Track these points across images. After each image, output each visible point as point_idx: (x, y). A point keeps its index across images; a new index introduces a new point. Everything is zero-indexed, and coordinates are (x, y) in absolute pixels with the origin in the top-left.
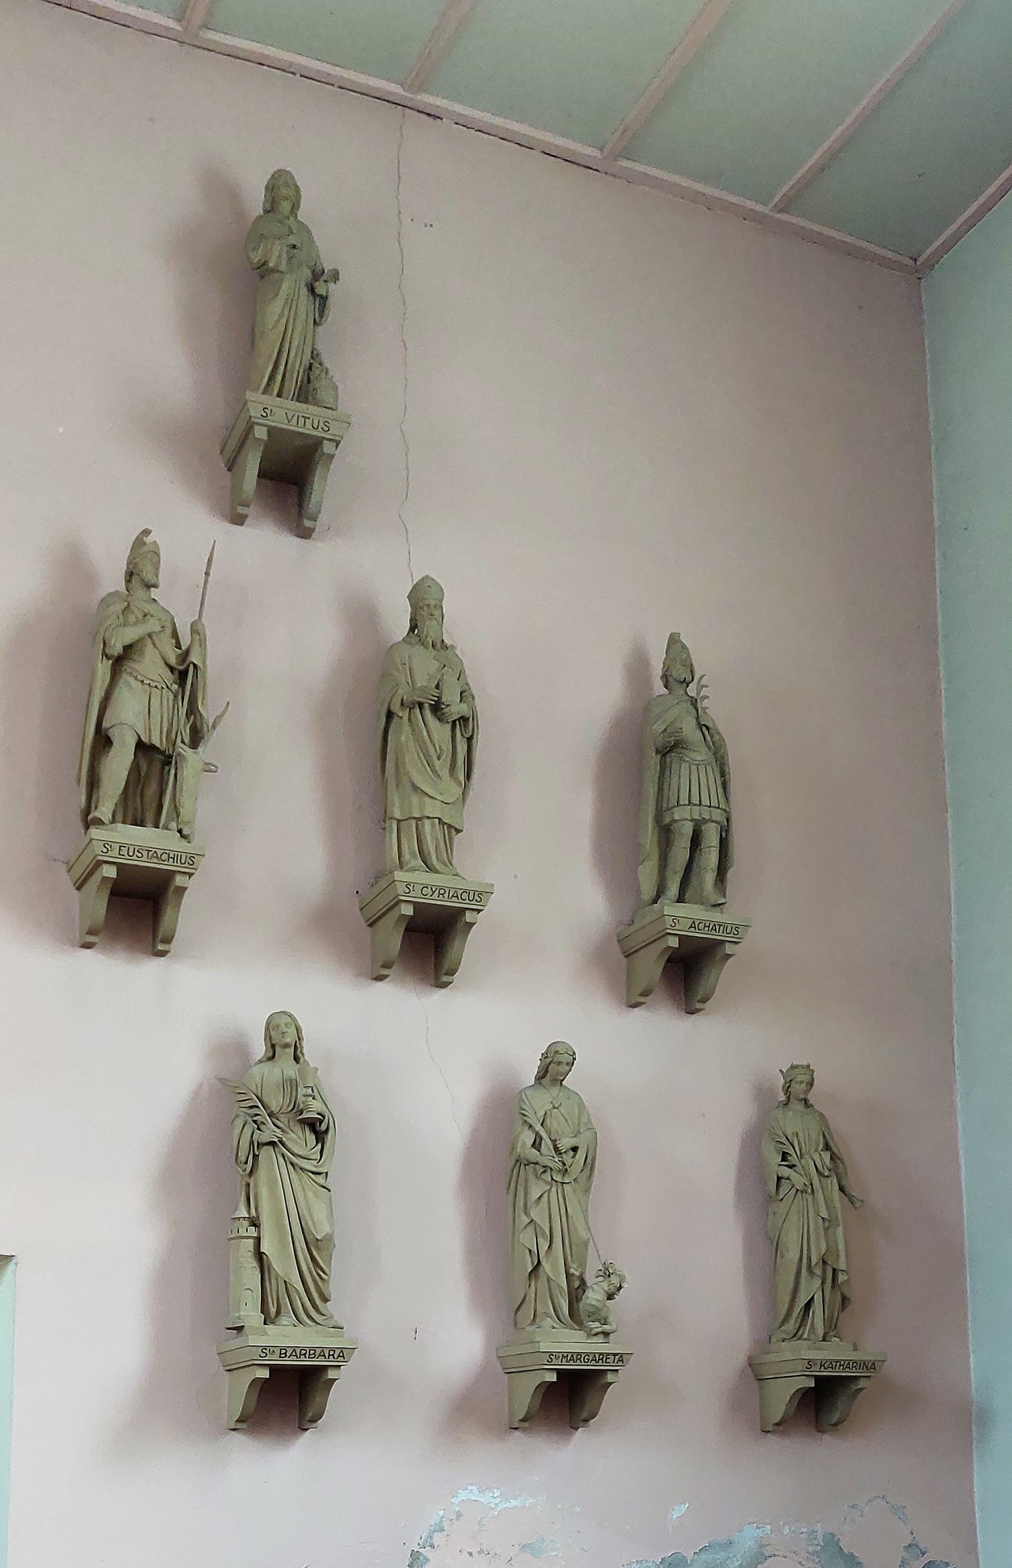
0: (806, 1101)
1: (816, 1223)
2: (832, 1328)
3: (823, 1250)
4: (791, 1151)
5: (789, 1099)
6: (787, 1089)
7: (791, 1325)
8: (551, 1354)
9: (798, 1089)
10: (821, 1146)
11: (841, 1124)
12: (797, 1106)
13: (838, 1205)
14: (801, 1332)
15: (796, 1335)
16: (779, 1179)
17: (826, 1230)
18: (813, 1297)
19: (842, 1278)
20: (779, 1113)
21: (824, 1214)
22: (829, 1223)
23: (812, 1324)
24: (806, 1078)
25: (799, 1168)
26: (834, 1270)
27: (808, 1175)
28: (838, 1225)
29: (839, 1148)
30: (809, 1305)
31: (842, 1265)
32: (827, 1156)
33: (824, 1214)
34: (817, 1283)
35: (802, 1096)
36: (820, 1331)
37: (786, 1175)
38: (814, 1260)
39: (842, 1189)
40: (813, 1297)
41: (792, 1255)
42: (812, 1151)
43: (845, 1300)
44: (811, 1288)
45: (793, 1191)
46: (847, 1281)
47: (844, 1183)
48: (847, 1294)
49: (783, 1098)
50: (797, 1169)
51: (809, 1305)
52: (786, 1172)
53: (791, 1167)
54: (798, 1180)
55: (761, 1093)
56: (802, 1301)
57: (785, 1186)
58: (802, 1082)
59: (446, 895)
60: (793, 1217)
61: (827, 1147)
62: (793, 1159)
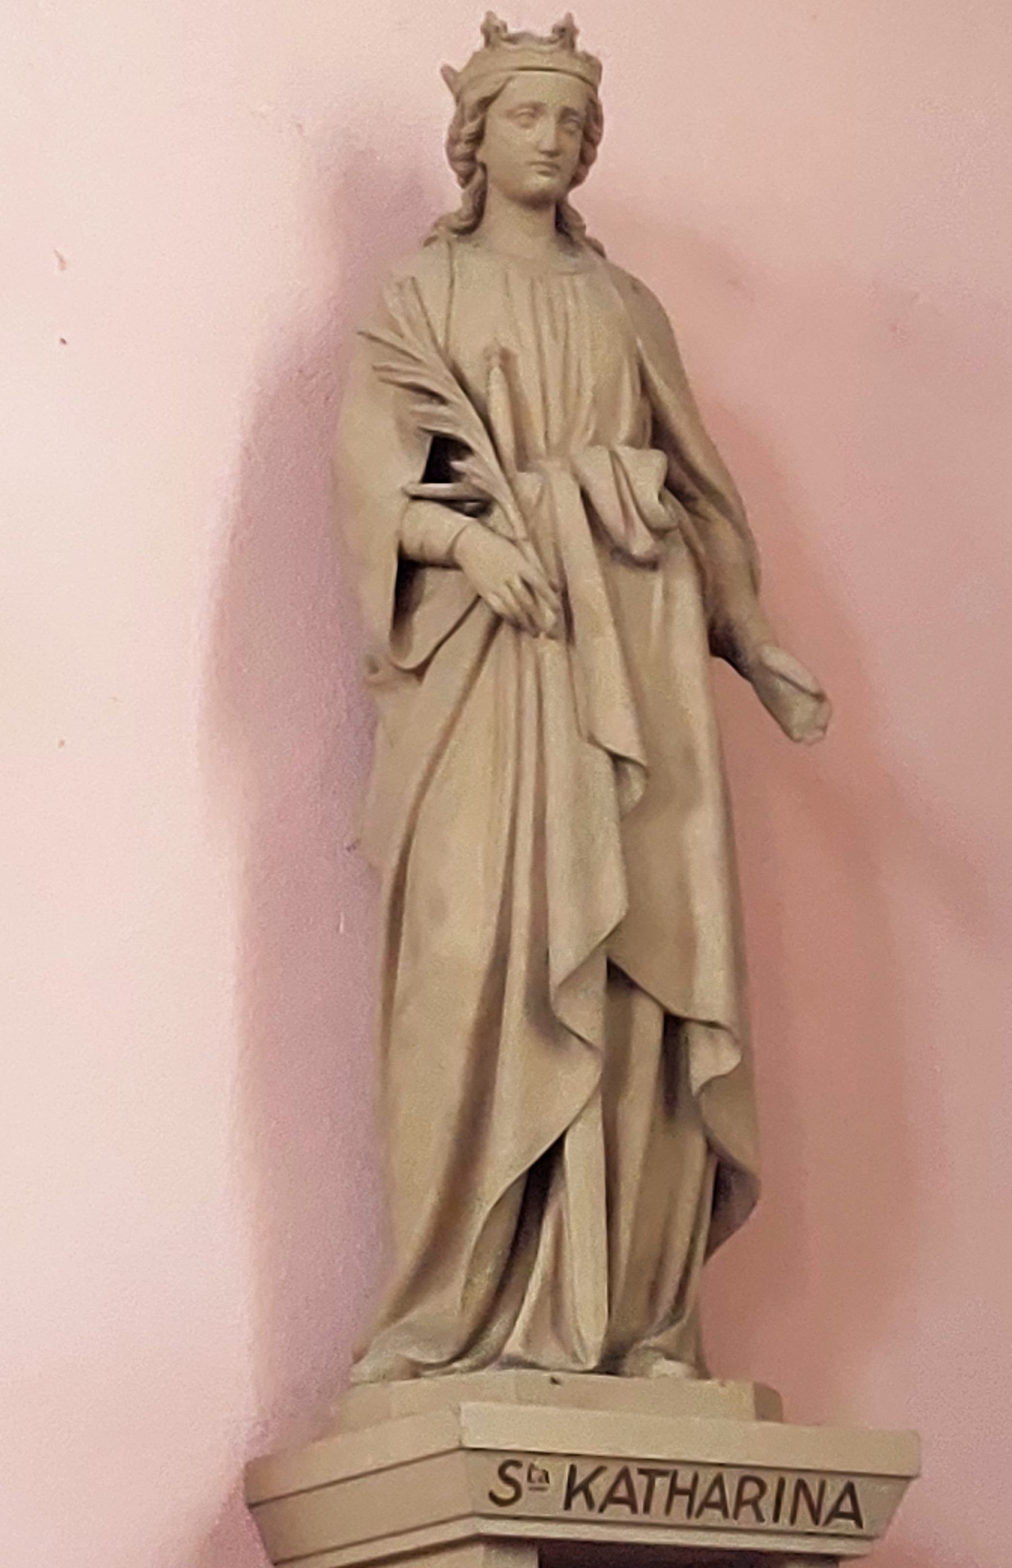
0: (564, 226)
1: (579, 776)
2: (655, 1317)
3: (612, 905)
4: (473, 436)
5: (479, 212)
6: (470, 151)
7: (451, 1303)
8: (507, 1464)
9: (521, 146)
10: (625, 425)
11: (741, 383)
12: (512, 230)
13: (697, 711)
14: (497, 1330)
15: (472, 1346)
16: (410, 569)
17: (630, 819)
18: (558, 1146)
19: (708, 1061)
20: (429, 268)
21: (622, 734)
22: (642, 784)
23: (555, 1284)
24: (553, 90)
25: (506, 511)
26: (674, 1026)
27: (535, 537)
28: (689, 803)
29: (716, 448)
30: (542, 1177)
31: (710, 994)
32: (648, 470)
33: (622, 734)
34: (583, 1075)
35: (539, 182)
36: (590, 1325)
37: (438, 547)
38: (564, 957)
39: (722, 644)
40: (558, 1146)
41: (458, 935)
42: (576, 447)
43: (727, 1187)
44: (545, 1099)
45: (479, 621)
46: (743, 1073)
47: (740, 609)
48: (741, 1150)
49: (454, 198)
50: (496, 517)
51: (542, 1177)
52: (438, 528)
53: (480, 507)
54: (492, 560)
55: (357, 197)
56: (502, 1170)
57: (438, 601)
58: (536, 110)
59: (767, 1505)
60: (473, 754)
61: (658, 433)
62: (480, 468)
